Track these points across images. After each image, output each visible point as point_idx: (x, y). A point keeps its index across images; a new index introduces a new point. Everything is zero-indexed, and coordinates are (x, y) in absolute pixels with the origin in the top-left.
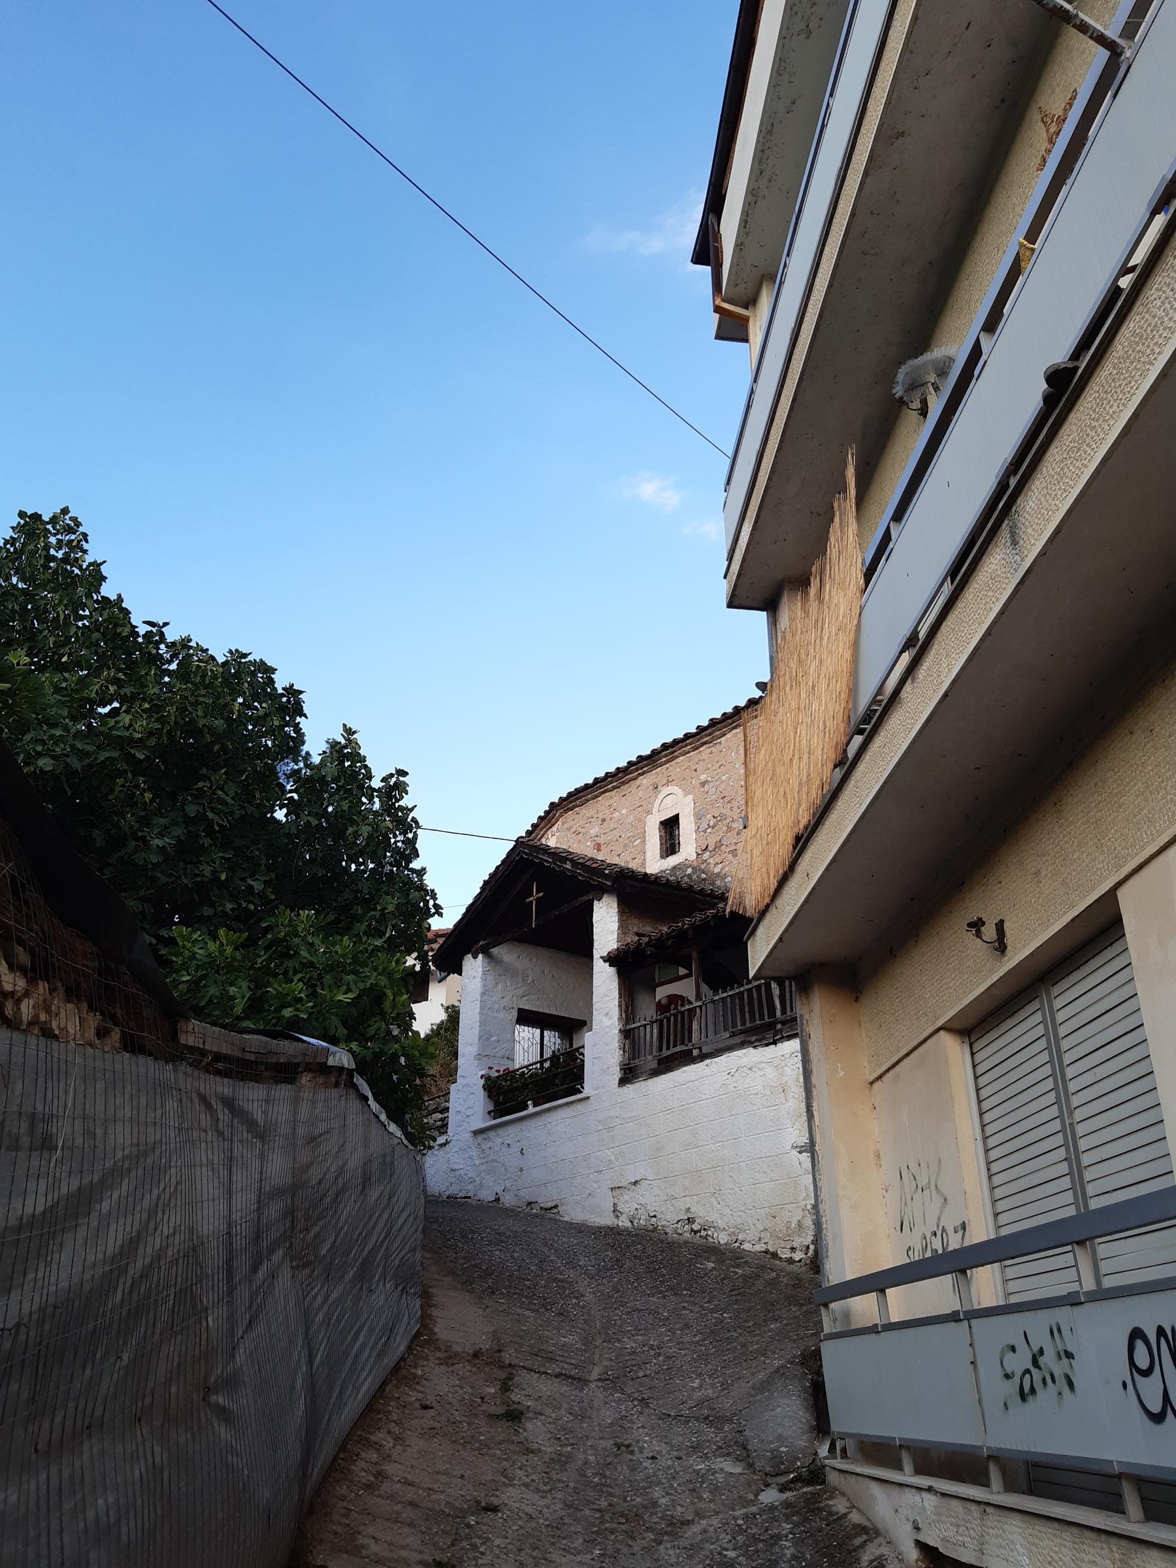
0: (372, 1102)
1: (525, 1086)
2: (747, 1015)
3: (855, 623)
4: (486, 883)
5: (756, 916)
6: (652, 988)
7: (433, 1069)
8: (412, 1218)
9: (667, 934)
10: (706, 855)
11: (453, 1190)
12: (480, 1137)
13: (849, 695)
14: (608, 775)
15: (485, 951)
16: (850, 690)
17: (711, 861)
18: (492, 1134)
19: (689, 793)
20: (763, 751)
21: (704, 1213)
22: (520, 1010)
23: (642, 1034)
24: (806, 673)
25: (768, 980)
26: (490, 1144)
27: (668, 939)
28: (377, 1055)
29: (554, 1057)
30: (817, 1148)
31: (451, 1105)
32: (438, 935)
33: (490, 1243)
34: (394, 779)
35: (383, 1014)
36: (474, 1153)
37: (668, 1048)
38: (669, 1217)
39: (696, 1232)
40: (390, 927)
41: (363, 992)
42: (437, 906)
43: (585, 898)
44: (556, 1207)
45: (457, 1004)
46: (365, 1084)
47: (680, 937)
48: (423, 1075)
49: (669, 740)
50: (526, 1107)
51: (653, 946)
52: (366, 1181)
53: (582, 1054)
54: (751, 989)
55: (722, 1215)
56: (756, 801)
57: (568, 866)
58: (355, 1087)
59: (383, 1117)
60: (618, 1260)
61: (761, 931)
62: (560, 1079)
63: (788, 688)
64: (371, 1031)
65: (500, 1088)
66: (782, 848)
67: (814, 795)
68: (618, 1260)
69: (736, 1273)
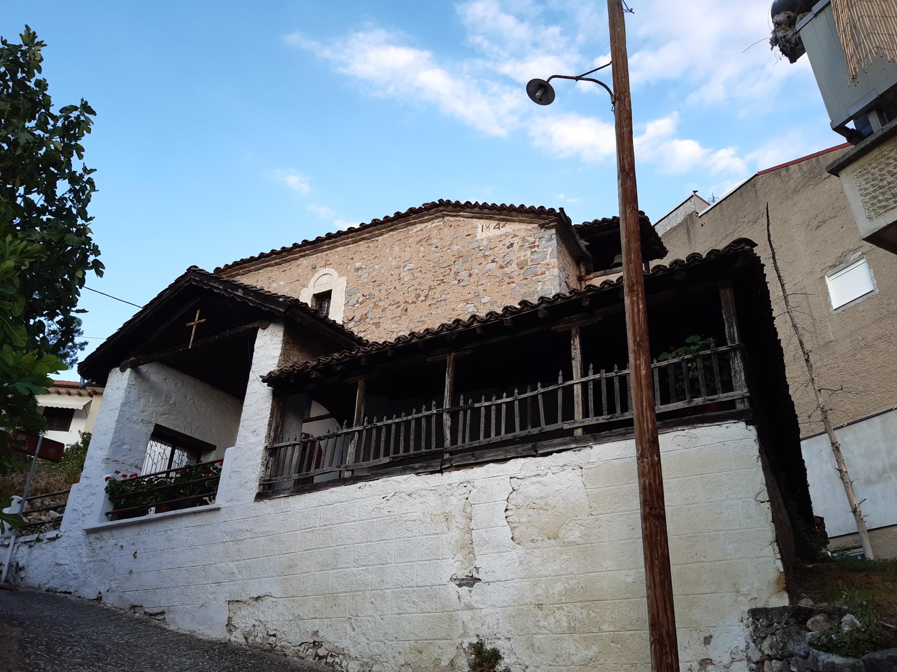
1: (150, 492)
9: (338, 360)
11: (55, 584)
14: (273, 252)
15: (135, 367)
18: (106, 535)
19: (343, 275)
22: (157, 426)
26: (102, 544)
27: (338, 365)
36: (84, 551)
37: (377, 456)
39: (321, 658)
43: (250, 326)
44: (163, 613)
54: (390, 425)
55: (356, 643)
57: (240, 293)
62: (193, 486)
65: (123, 491)
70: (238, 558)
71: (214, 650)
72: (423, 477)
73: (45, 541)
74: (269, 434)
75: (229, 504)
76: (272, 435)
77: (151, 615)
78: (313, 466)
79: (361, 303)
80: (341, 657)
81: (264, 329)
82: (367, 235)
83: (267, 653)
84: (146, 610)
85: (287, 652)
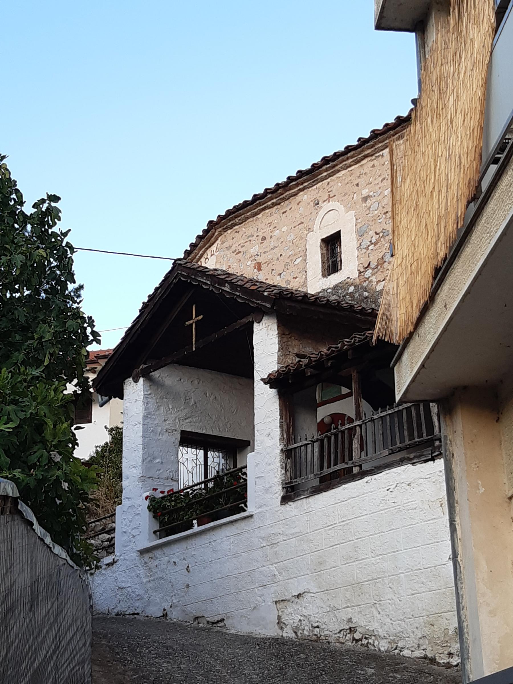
0: (37, 527)
1: (190, 506)
2: (406, 433)
3: (487, 61)
4: (145, 306)
5: (401, 343)
6: (313, 407)
7: (97, 493)
8: (79, 634)
9: (327, 355)
10: (369, 272)
12: (147, 557)
13: (481, 133)
15: (146, 375)
16: (482, 128)
17: (373, 278)
18: (158, 553)
19: (350, 209)
20: (408, 181)
21: (365, 622)
22: (183, 432)
23: (303, 454)
24: (445, 106)
25: (417, 404)
26: (157, 562)
27: (328, 360)
28: (40, 482)
29: (218, 478)
30: (459, 559)
31: (117, 525)
32: (99, 356)
33: (158, 656)
34: (46, 205)
35: (44, 442)
36: (142, 571)
37: (329, 467)
38: (331, 627)
39: (357, 641)
40: (48, 355)
41: (23, 421)
42: (93, 333)
43: (245, 320)
45: (120, 426)
46: (29, 510)
47: (340, 358)
48: (86, 500)
49: (330, 153)
50: (191, 526)
51: (311, 367)
52: (34, 600)
53: (245, 474)
55: (382, 625)
56: (401, 231)
57: (227, 288)
58: (20, 513)
59: (48, 540)
60: (281, 669)
61: (405, 357)
62: (225, 497)
63: (429, 120)
64: (34, 459)
65: (164, 508)
66: (423, 280)
67: (450, 229)
68: (281, 669)
69: (395, 678)
70: (277, 561)
71: (266, 643)
72: (419, 466)
73: (104, 567)
74: (283, 436)
75: (260, 509)
76: (285, 436)
77: (213, 623)
78: (325, 465)
79: (375, 244)
80: (373, 638)
81: (259, 323)
82: (369, 151)
83: (314, 643)
84: (208, 619)
85: (330, 640)
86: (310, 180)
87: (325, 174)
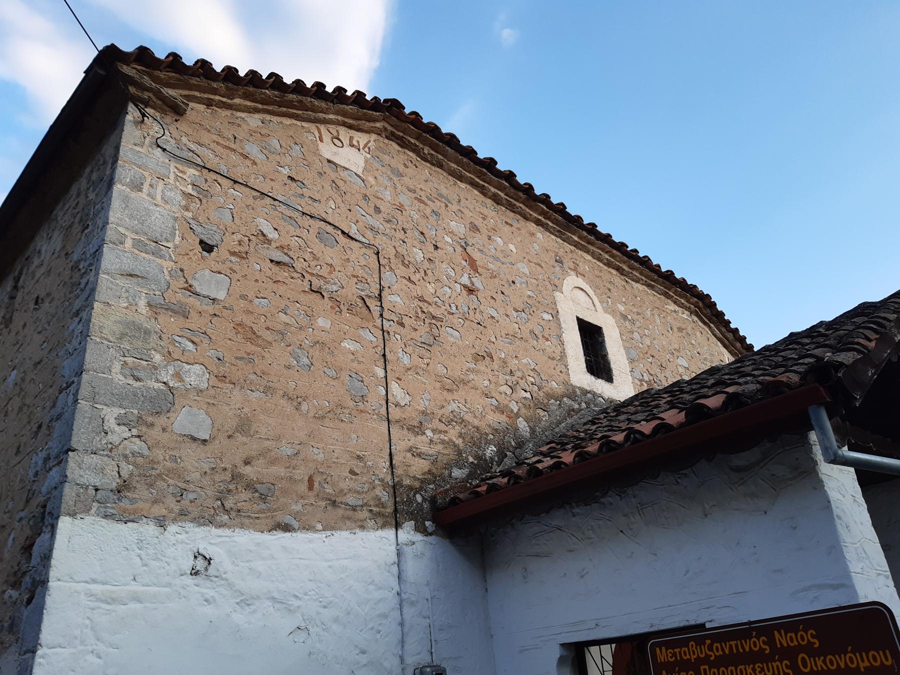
82: (625, 267)
86: (557, 225)
87: (576, 238)
